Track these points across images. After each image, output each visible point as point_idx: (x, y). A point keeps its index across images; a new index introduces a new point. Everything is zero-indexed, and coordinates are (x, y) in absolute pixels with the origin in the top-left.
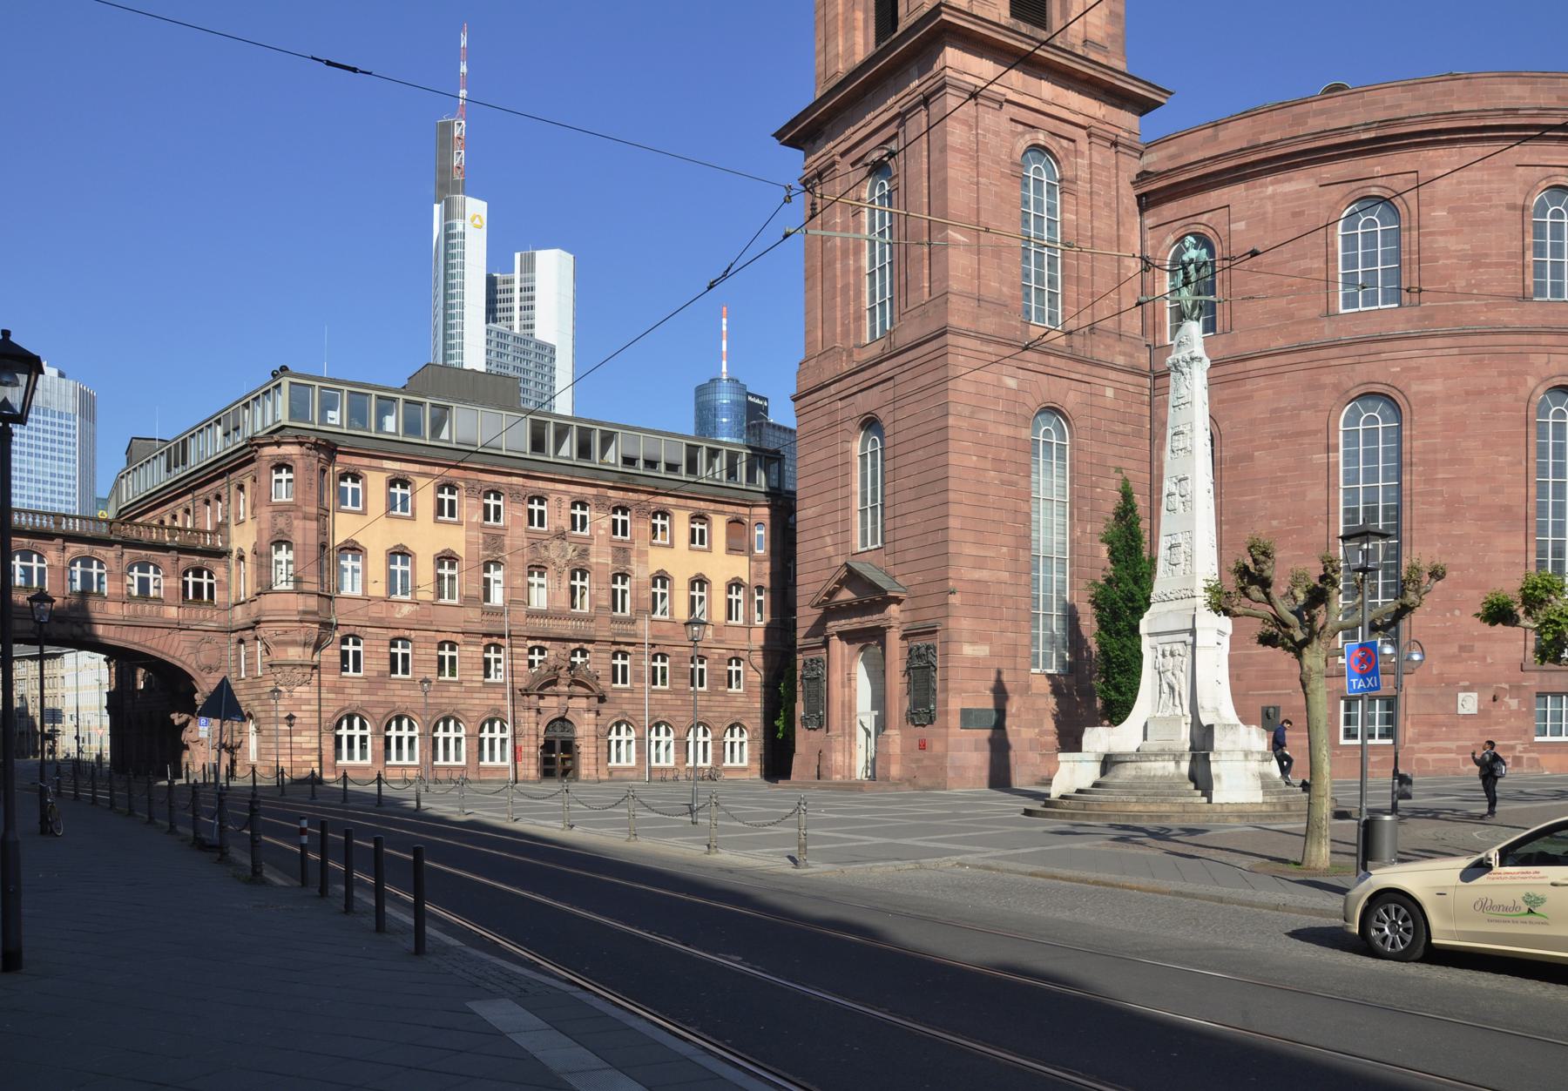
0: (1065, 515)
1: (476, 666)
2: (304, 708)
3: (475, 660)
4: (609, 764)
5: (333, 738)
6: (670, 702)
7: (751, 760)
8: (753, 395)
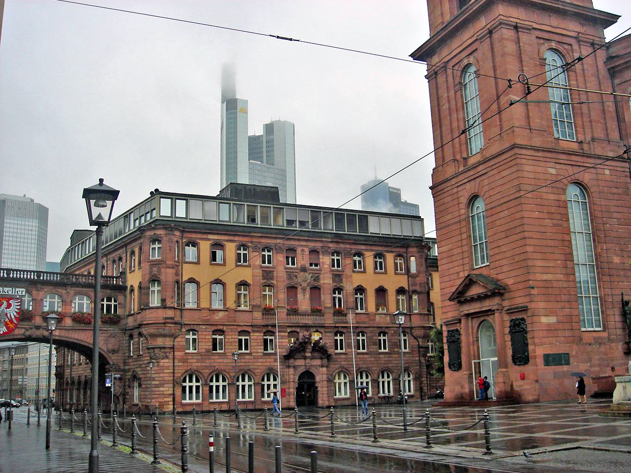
0: (591, 241)
1: (259, 344)
2: (165, 371)
3: (259, 341)
4: (379, 395)
5: (181, 388)
6: (368, 359)
7: (415, 390)
8: (392, 188)
